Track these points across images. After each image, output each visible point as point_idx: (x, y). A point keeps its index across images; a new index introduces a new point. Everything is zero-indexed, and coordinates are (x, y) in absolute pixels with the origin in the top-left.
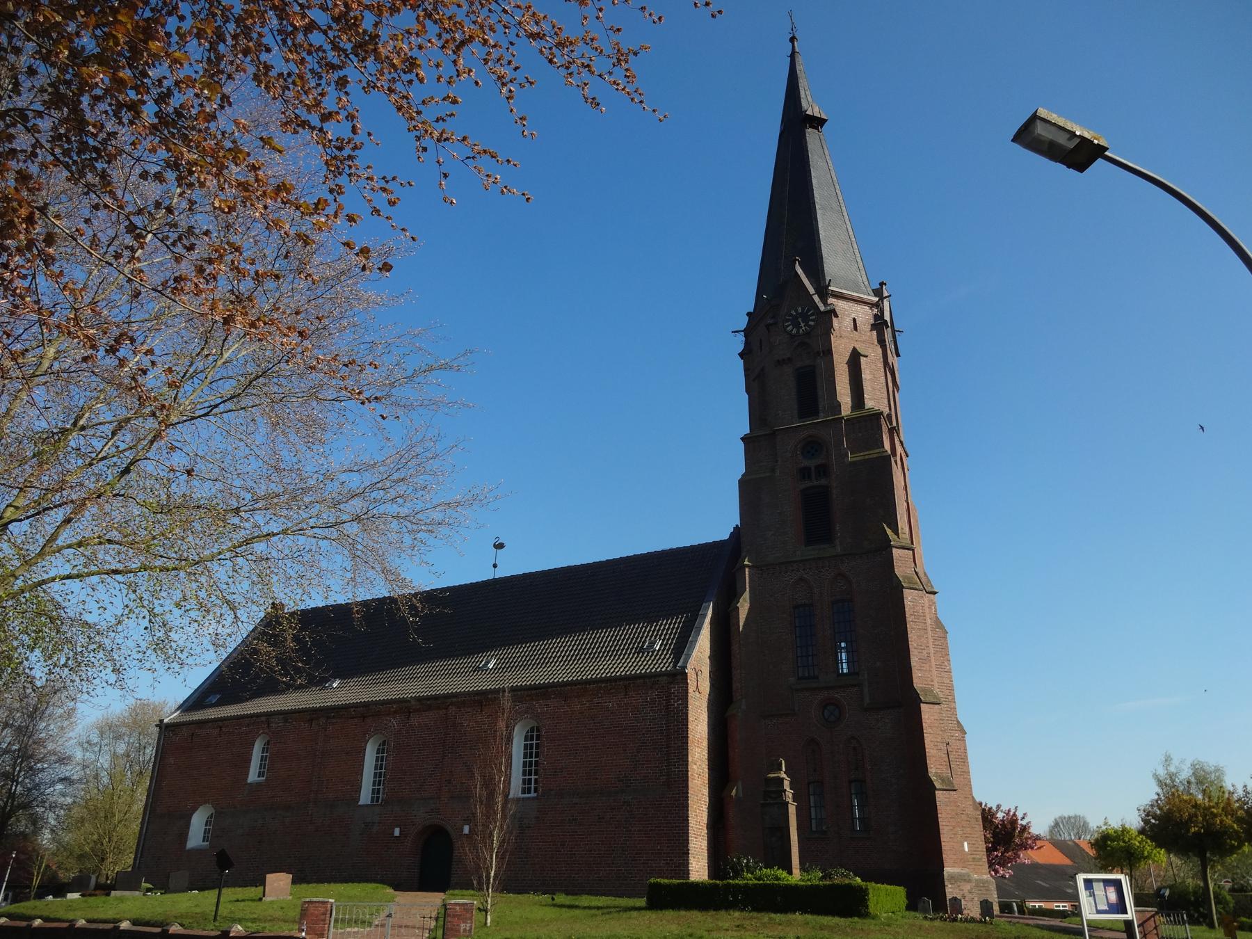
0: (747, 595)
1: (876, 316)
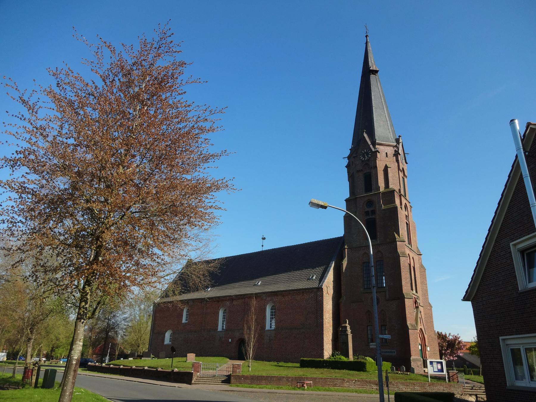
0: (346, 259)
1: (395, 151)
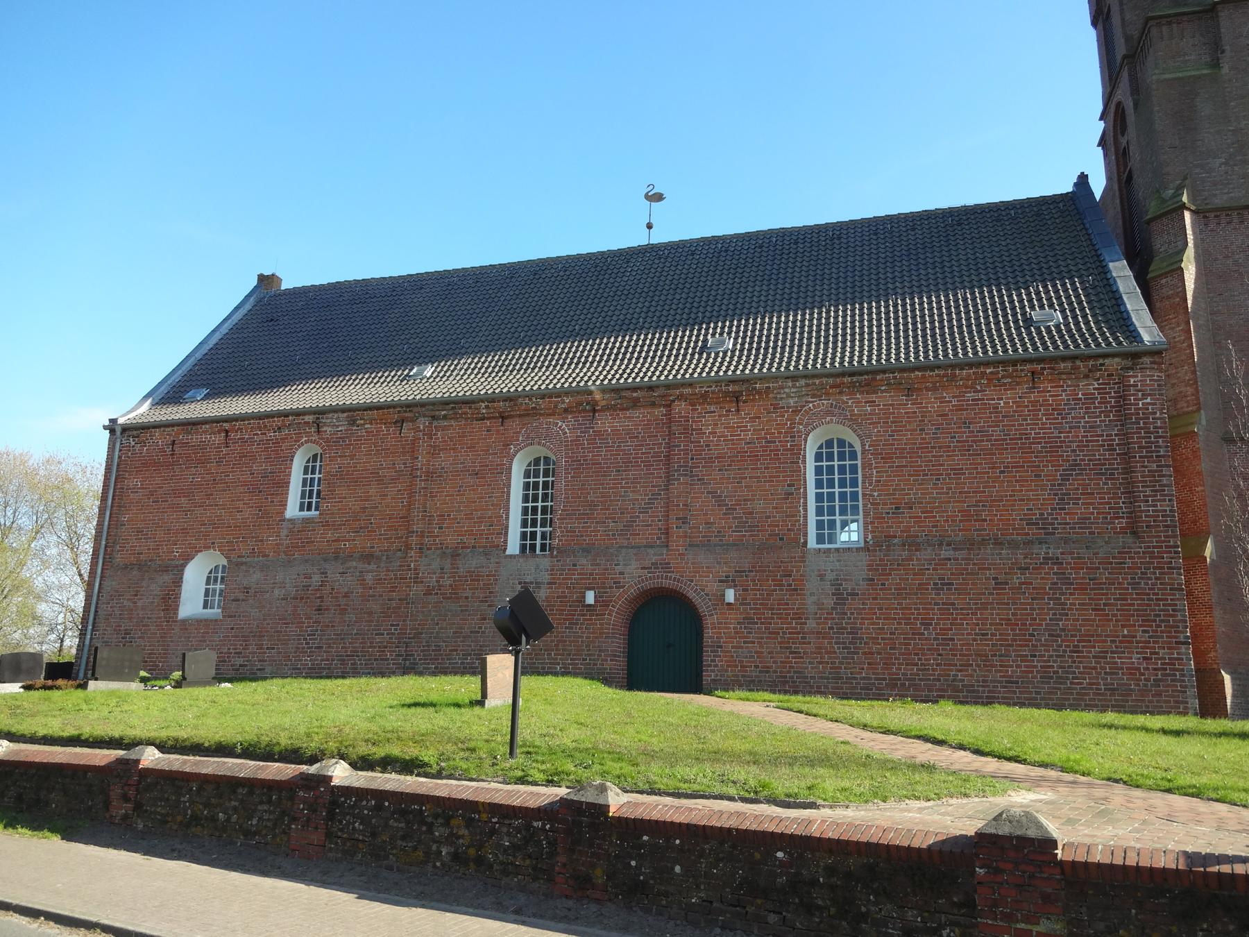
0: (1190, 252)
